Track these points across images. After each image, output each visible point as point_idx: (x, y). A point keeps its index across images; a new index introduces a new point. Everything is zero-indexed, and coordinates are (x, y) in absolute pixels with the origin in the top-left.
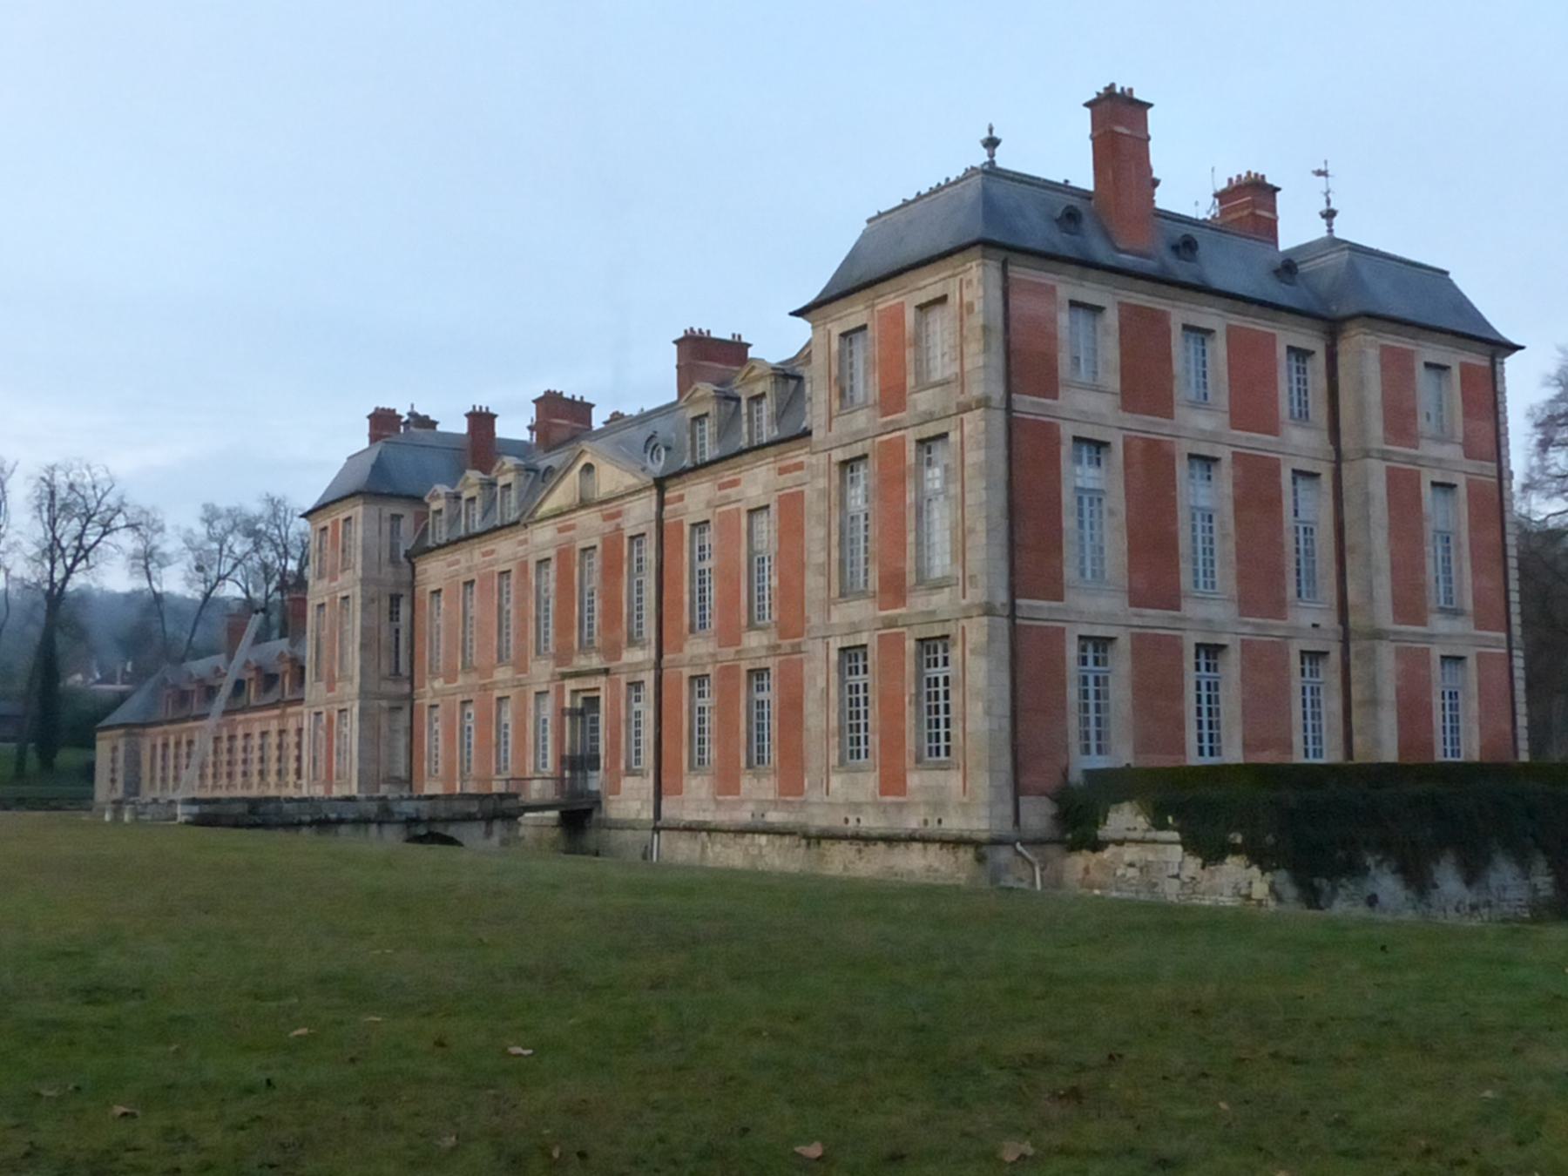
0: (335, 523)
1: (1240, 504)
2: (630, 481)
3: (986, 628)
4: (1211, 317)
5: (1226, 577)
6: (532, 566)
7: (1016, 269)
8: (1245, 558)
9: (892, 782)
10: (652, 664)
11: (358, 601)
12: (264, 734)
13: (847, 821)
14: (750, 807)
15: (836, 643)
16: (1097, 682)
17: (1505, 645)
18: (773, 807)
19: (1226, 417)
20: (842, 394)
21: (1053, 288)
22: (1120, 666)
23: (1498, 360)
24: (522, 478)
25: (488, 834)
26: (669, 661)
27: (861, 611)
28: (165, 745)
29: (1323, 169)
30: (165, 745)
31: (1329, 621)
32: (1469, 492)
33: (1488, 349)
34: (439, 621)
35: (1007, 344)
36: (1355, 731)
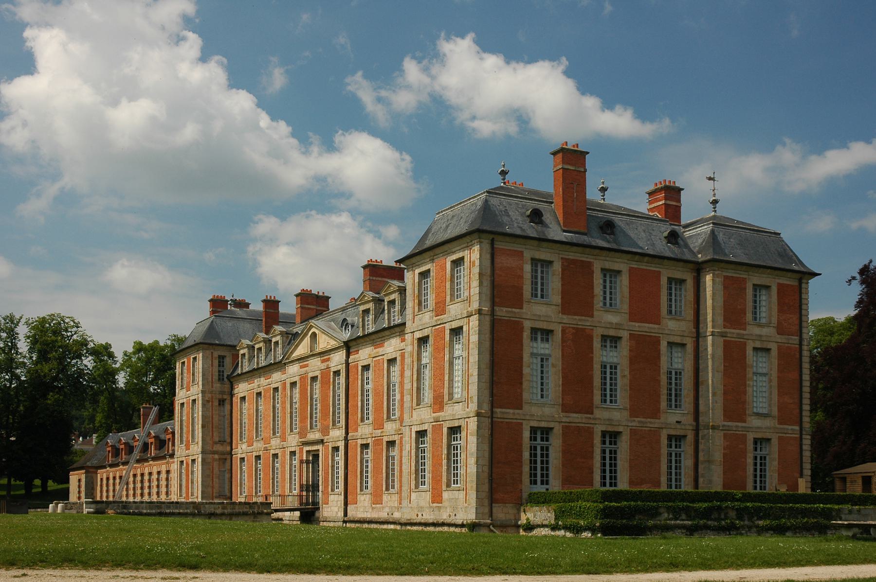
2: (333, 343)
4: (621, 265)
5: (622, 397)
6: (288, 386)
7: (500, 243)
8: (635, 389)
9: (437, 498)
11: (200, 402)
12: (159, 473)
15: (415, 429)
17: (799, 432)
18: (396, 510)
19: (627, 316)
20: (420, 304)
21: (522, 252)
22: (556, 444)
23: (804, 281)
24: (285, 338)
26: (352, 436)
28: (108, 479)
29: (712, 177)
30: (108, 479)
31: (689, 420)
32: (779, 353)
33: (798, 276)
34: (244, 413)
35: (493, 282)
36: (700, 475)
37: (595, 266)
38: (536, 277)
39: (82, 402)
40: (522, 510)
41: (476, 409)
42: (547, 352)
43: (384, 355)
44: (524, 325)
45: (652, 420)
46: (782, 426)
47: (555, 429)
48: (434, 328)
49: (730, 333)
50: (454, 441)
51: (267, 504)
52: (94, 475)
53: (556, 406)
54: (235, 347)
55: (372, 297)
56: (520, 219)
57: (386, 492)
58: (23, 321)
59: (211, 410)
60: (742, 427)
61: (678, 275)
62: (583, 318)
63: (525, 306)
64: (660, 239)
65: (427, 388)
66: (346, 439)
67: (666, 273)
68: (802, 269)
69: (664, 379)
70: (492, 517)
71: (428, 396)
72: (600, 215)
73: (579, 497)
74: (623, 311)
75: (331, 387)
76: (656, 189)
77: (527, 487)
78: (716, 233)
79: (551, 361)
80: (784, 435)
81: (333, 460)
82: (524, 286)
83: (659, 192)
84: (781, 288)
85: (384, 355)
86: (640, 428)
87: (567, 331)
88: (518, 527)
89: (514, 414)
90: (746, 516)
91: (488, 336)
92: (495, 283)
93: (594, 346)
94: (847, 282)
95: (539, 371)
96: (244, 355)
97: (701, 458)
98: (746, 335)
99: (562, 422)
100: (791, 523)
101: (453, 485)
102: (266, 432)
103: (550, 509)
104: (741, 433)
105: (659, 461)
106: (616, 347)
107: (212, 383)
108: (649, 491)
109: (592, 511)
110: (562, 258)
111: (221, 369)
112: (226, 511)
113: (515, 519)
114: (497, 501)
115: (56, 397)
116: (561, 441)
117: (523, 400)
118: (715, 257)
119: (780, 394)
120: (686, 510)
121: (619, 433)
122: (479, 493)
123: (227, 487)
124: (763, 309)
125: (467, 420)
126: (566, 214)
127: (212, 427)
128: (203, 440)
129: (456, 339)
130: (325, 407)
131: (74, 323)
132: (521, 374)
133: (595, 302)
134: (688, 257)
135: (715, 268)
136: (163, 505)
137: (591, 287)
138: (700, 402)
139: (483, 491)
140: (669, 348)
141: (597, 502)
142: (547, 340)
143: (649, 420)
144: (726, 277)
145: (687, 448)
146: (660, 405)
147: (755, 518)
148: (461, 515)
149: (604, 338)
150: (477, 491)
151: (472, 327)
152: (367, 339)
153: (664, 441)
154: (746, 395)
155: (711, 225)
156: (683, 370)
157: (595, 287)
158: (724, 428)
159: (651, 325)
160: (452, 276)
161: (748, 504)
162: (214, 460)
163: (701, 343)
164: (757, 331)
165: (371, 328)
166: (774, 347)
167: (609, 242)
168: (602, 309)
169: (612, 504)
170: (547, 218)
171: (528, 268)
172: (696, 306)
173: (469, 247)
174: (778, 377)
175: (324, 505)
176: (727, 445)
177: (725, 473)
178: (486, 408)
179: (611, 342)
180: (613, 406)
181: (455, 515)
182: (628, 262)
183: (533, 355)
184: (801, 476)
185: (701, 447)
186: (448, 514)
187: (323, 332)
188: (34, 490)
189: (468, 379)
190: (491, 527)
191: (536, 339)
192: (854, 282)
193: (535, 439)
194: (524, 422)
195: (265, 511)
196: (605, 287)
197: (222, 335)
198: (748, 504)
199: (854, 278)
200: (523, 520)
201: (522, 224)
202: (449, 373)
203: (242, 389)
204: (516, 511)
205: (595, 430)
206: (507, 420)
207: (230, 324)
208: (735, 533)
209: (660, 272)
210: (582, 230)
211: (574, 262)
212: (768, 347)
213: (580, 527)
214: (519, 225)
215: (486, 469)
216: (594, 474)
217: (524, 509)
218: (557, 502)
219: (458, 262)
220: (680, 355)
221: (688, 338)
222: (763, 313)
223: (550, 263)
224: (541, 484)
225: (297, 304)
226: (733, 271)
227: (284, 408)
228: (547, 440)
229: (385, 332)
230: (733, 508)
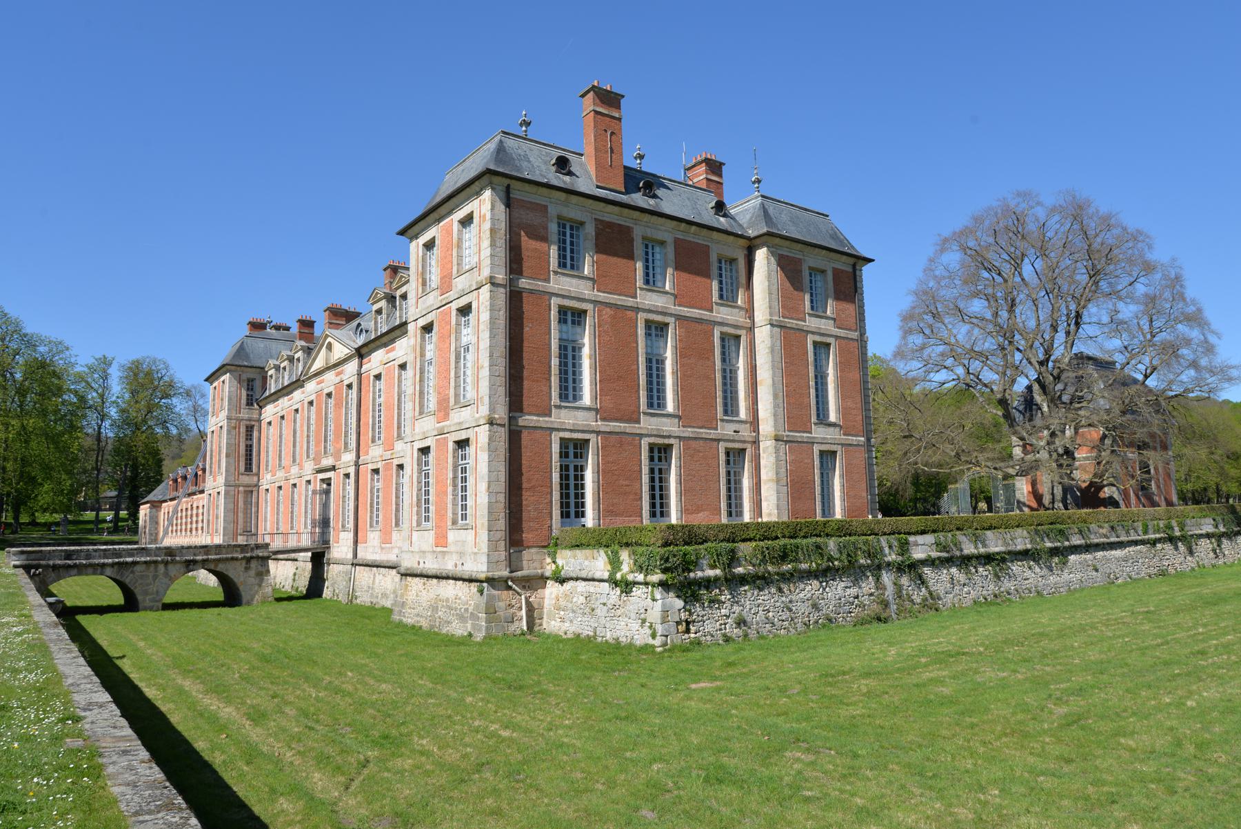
0: (219, 383)
6: (306, 405)
9: (441, 540)
10: (352, 463)
13: (419, 563)
14: (396, 551)
20: (424, 284)
21: (546, 207)
23: (857, 267)
25: (247, 569)
27: (428, 425)
50: (462, 460)
54: (263, 368)
55: (384, 293)
66: (357, 465)
68: (855, 253)
71: (432, 403)
81: (344, 489)
84: (836, 273)
96: (271, 376)
101: (424, 523)
128: (226, 471)
130: (338, 427)
181: (463, 564)
197: (251, 356)
209: (709, 246)
211: (610, 225)
227: (302, 431)
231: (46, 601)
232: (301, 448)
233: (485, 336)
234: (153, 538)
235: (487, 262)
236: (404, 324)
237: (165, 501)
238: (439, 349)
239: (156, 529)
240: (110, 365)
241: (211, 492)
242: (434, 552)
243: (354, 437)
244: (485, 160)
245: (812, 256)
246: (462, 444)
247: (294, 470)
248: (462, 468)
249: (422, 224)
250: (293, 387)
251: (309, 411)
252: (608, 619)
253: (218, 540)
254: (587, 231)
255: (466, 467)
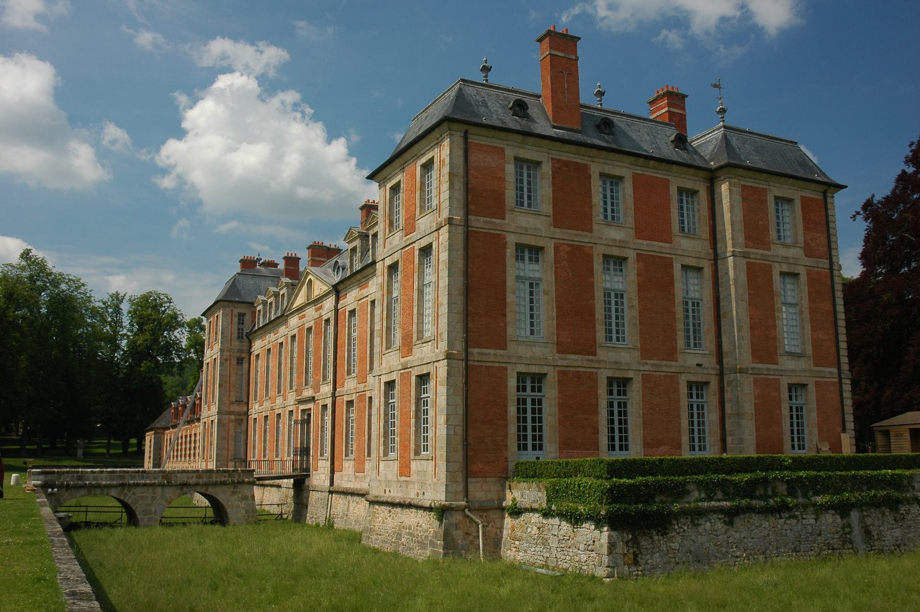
1: (642, 288)
3: (446, 367)
4: (622, 168)
5: (631, 334)
6: (289, 339)
7: (476, 137)
8: (646, 323)
9: (405, 470)
16: (619, 406)
17: (837, 376)
19: (632, 232)
20: (391, 224)
21: (503, 150)
22: (550, 394)
23: (829, 195)
29: (718, 84)
31: (710, 362)
33: (821, 188)
35: (467, 184)
36: (728, 433)
37: (592, 169)
38: (522, 181)
39: (170, 369)
40: (507, 486)
41: (446, 348)
42: (537, 275)
43: (367, 296)
44: (507, 240)
45: (668, 363)
46: (818, 368)
47: (548, 375)
48: (403, 251)
49: (753, 253)
50: (424, 393)
51: (249, 471)
52: (162, 436)
53: (549, 345)
54: (252, 303)
55: (359, 232)
56: (500, 111)
57: (368, 458)
58: (127, 298)
59: (228, 369)
60: (774, 370)
61: (689, 185)
62: (580, 232)
63: (507, 216)
64: (666, 143)
65: (397, 328)
66: (334, 396)
67: (676, 181)
68: (826, 180)
69: (679, 310)
70: (467, 497)
72: (596, 113)
73: (578, 470)
74: (628, 226)
75: (323, 337)
76: (658, 97)
77: (514, 455)
78: (729, 138)
79: (542, 286)
80: (821, 379)
82: (507, 191)
83: (661, 99)
84: (805, 201)
85: (367, 296)
86: (654, 373)
87: (561, 249)
88: (503, 509)
89: (495, 355)
90: (799, 491)
91: (461, 252)
92: (470, 186)
93: (595, 268)
94: (851, 218)
95: (528, 300)
96: (259, 311)
97: (728, 410)
98: (771, 256)
99: (557, 366)
100: (855, 497)
101: (422, 453)
102: (273, 391)
103: (541, 487)
104: (773, 377)
105: (679, 416)
106: (621, 270)
107: (231, 341)
108: (672, 460)
109: (594, 492)
110: (552, 158)
111: (241, 327)
112: (201, 481)
113: (499, 499)
114: (475, 475)
115: (148, 364)
116: (557, 392)
117: (508, 337)
118: (730, 161)
119: (813, 329)
120: (722, 484)
121: (629, 380)
122: (450, 464)
123: (243, 449)
124: (787, 227)
125: (436, 364)
126: (556, 107)
127: (229, 387)
129: (427, 261)
130: (317, 359)
131: (168, 298)
132: (504, 304)
133: (593, 214)
134: (699, 163)
135: (731, 176)
136: (127, 475)
137: (588, 194)
138: (723, 340)
139: (455, 462)
140: (684, 273)
141: (601, 478)
142: (537, 260)
143: (664, 362)
144: (744, 187)
145: (711, 397)
146: (676, 344)
147: (811, 493)
148: (430, 494)
149: (607, 258)
150: (448, 461)
151: (442, 242)
152: (353, 280)
153: (684, 390)
154: (775, 330)
155: (723, 129)
156: (701, 300)
157: (593, 195)
158: (754, 372)
159: (661, 243)
160: (422, 184)
161: (801, 473)
162: (230, 421)
163: (720, 267)
164: (782, 252)
165: (357, 266)
166: (802, 271)
167: (607, 142)
168: (602, 222)
169: (622, 481)
170: (533, 111)
171: (510, 168)
172: (711, 221)
173: (438, 144)
174: (810, 308)
175: (314, 472)
176: (759, 393)
177: (757, 430)
178: (459, 346)
179: (615, 263)
180: (620, 344)
181: (424, 493)
182: (631, 167)
183: (518, 278)
184: (844, 430)
185: (727, 396)
186: (416, 491)
187: (317, 279)
188: (130, 450)
189: (438, 309)
190: (466, 510)
191: (523, 259)
192: (859, 218)
193: (524, 390)
194: (509, 367)
195: (247, 480)
196: (605, 196)
198: (801, 473)
199: (858, 213)
200: (508, 503)
201: (503, 116)
202: (418, 305)
203: (258, 346)
204: (500, 488)
205: (599, 375)
206: (487, 364)
207: (252, 282)
208: (787, 515)
209: (668, 180)
210: (575, 127)
211: (566, 163)
212: (797, 272)
213: (580, 516)
214: (499, 117)
215: (459, 430)
216: (600, 434)
217: (510, 485)
218: (549, 477)
219: (428, 166)
220: (696, 281)
221: (705, 261)
222: (788, 233)
223: (539, 164)
224: (533, 450)
225: (309, 257)
226: (751, 180)
227: (286, 363)
228: (540, 390)
229: (368, 269)
230: (782, 480)
231: (55, 516)
232: (285, 379)
233: (444, 273)
234: (157, 462)
235: (446, 204)
236: (374, 263)
237: (168, 428)
238: (404, 287)
239: (160, 454)
240: (121, 301)
241: (205, 420)
242: (398, 481)
243: (331, 370)
244: (445, 108)
245: (778, 185)
246: (423, 379)
247: (279, 401)
248: (424, 401)
249: (388, 169)
250: (278, 321)
251: (308, 337)
252: (559, 550)
253: (212, 466)
254: (543, 170)
255: (427, 400)
